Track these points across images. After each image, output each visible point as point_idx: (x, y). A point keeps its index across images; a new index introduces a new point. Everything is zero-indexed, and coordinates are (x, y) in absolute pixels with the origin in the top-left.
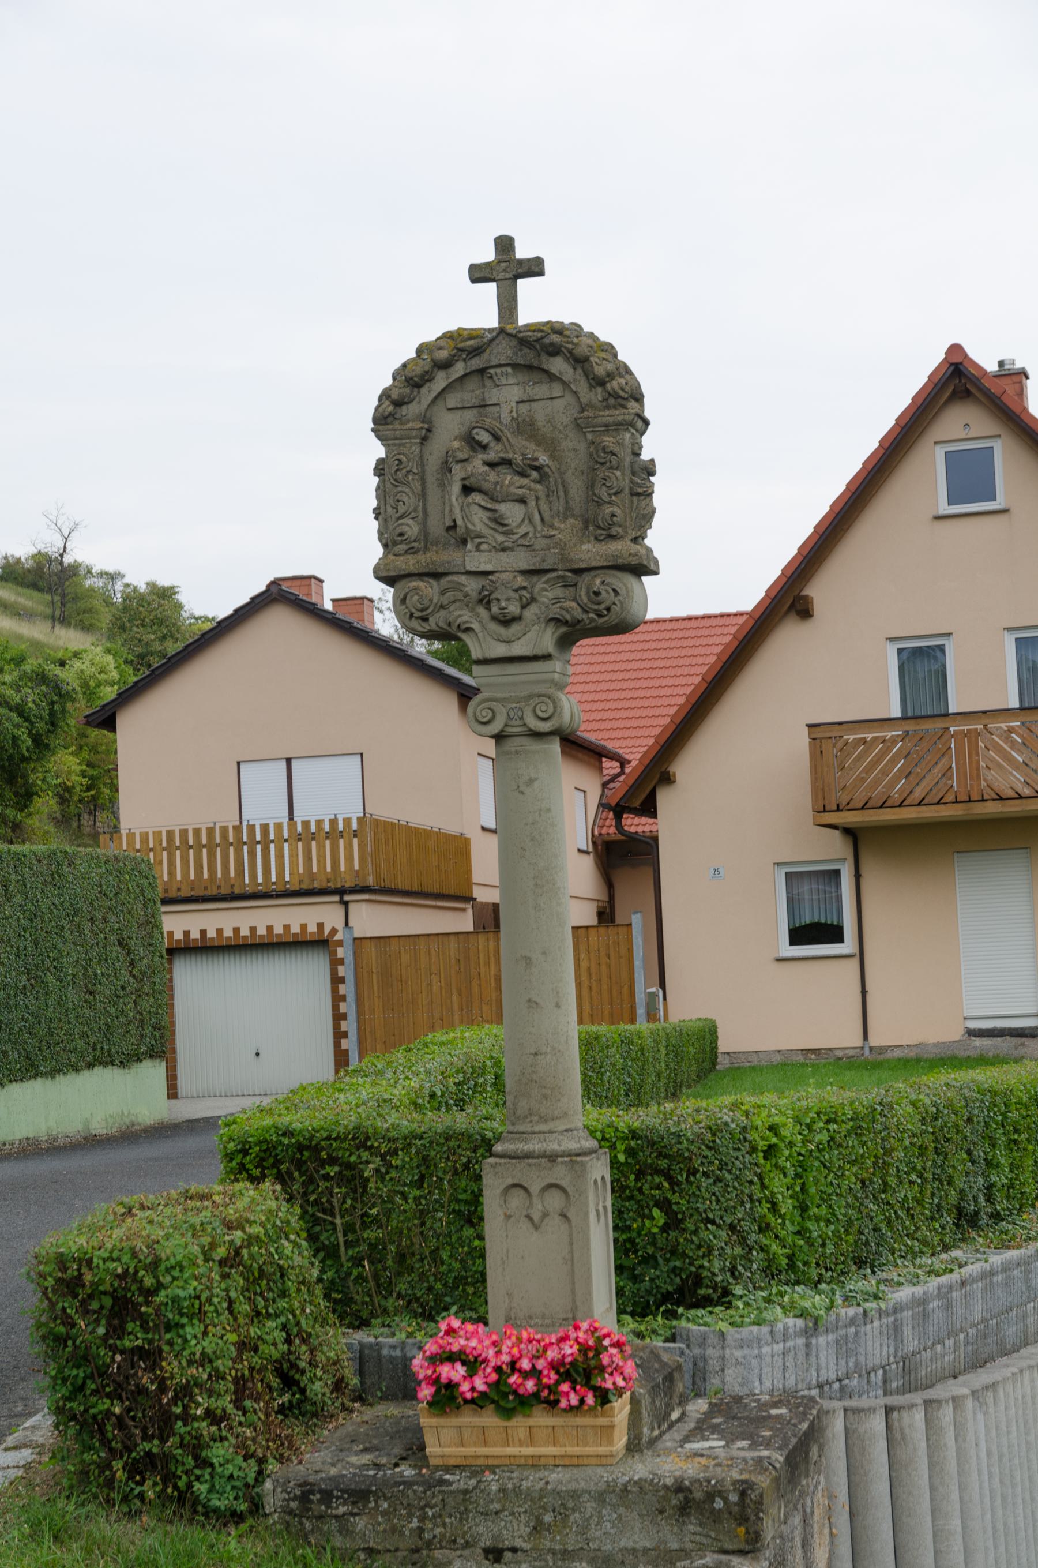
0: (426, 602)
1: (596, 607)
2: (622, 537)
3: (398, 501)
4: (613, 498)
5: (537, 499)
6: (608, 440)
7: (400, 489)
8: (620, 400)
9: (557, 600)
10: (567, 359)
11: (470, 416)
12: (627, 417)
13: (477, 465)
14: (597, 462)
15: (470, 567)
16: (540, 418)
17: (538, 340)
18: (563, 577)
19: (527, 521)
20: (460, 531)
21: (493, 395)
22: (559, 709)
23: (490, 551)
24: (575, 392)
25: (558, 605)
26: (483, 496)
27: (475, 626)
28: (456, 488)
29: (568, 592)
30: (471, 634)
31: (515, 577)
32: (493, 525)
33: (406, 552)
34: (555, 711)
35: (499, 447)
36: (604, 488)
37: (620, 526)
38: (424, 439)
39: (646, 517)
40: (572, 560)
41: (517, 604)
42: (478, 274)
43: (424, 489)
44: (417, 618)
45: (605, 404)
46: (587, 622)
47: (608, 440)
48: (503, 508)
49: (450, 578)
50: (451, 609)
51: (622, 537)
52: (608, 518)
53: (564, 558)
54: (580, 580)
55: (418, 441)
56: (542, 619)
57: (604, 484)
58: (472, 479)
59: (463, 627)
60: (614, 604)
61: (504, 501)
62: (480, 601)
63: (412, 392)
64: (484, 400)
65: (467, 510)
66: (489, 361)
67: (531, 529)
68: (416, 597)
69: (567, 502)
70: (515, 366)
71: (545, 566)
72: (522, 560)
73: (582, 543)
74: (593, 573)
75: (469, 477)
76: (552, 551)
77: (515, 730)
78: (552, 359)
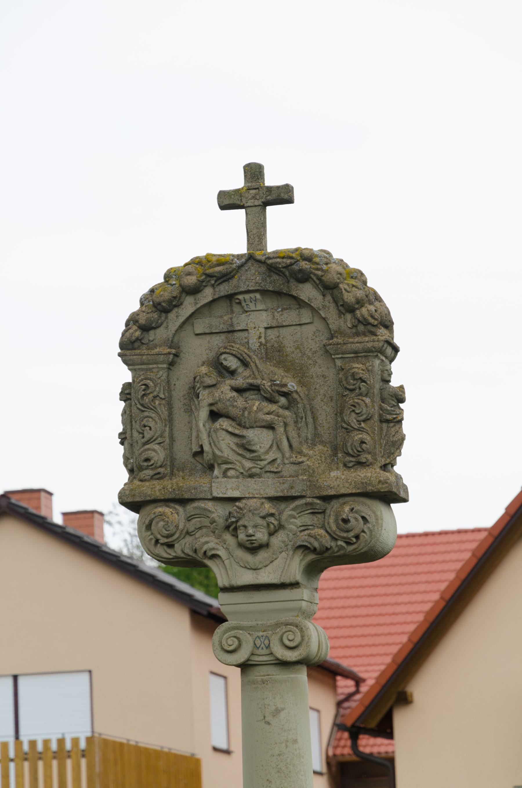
0: (172, 528)
1: (345, 535)
2: (371, 464)
3: (145, 426)
4: (363, 425)
5: (286, 425)
6: (357, 367)
7: (146, 414)
8: (369, 327)
9: (305, 527)
10: (316, 286)
11: (218, 341)
12: (376, 344)
13: (225, 391)
14: (346, 389)
16: (289, 346)
17: (287, 267)
18: (311, 504)
19: (275, 448)
20: (207, 457)
21: (242, 321)
22: (306, 638)
23: (237, 477)
24: (324, 319)
25: (306, 532)
26: (231, 422)
27: (222, 553)
28: (203, 414)
29: (317, 519)
30: (218, 561)
31: (263, 503)
33: (152, 478)
34: (302, 640)
35: (247, 373)
36: (353, 414)
37: (369, 453)
38: (172, 364)
40: (320, 487)
41: (265, 531)
42: (228, 201)
44: (162, 544)
45: (354, 330)
46: (336, 549)
47: (357, 367)
48: (251, 434)
49: (196, 504)
50: (197, 535)
51: (371, 464)
52: (357, 444)
55: (165, 366)
56: (289, 547)
57: (353, 411)
59: (210, 553)
60: (363, 531)
62: (227, 528)
63: (160, 317)
64: (232, 325)
67: (279, 455)
68: (162, 523)
69: (316, 428)
70: (264, 292)
71: (294, 493)
72: (270, 487)
74: (341, 500)
75: (216, 403)
76: (300, 477)
78: (301, 285)
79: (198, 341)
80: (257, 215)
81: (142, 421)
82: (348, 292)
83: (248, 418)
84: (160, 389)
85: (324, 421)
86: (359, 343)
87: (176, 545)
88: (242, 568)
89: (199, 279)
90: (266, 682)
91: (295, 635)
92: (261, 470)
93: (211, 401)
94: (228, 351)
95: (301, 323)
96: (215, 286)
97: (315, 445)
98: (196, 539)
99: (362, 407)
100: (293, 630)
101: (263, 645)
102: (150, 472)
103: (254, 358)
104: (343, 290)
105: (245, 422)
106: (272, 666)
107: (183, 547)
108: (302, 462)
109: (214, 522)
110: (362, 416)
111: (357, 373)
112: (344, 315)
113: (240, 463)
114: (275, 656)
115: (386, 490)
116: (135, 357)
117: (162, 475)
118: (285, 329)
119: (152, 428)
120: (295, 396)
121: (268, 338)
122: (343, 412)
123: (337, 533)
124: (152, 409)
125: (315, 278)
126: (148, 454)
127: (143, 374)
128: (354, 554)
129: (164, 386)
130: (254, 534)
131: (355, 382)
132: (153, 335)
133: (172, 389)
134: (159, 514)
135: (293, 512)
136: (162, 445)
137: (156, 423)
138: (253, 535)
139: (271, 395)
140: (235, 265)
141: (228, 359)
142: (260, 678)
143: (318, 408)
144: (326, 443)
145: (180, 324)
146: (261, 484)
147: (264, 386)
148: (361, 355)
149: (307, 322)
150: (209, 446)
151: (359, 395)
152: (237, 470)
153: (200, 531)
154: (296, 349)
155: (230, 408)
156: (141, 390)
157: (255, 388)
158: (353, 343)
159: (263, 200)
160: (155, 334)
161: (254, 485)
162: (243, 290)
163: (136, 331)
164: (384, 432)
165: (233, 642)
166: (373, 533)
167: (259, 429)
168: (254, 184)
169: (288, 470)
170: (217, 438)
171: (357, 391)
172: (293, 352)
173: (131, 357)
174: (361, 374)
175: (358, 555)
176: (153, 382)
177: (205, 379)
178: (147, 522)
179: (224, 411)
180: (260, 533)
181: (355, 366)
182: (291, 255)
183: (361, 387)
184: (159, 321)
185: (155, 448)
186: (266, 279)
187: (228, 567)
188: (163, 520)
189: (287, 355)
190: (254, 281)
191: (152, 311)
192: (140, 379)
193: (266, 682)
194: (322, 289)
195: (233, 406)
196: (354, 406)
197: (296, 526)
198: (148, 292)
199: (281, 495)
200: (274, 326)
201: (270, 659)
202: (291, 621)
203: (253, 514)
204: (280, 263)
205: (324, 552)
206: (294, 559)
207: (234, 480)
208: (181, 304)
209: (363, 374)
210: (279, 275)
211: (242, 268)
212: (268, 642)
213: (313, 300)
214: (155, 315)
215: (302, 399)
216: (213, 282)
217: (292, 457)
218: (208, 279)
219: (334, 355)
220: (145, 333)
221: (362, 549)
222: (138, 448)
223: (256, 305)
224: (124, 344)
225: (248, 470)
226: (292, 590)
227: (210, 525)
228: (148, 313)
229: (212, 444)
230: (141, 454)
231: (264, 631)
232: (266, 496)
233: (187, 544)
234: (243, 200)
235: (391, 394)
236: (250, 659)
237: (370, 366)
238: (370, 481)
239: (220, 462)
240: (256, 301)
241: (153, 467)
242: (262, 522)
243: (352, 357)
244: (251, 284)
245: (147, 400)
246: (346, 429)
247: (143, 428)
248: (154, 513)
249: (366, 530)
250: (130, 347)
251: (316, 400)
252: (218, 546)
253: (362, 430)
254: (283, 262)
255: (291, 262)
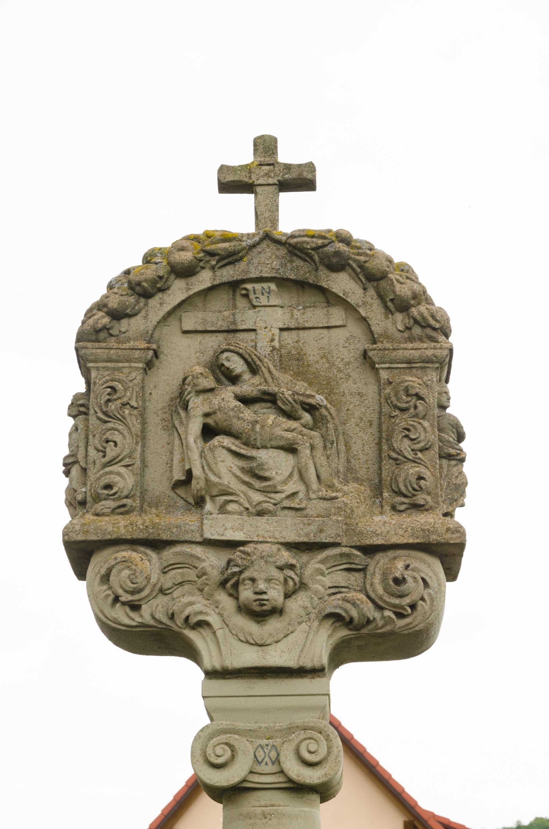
0: (141, 580)
1: (397, 601)
2: (431, 508)
3: (107, 441)
4: (420, 455)
5: (312, 447)
6: (412, 380)
7: (110, 425)
8: (428, 331)
9: (336, 589)
10: (355, 276)
11: (213, 342)
12: (438, 352)
13: (227, 396)
14: (396, 407)
15: (212, 532)
16: (312, 352)
17: (315, 249)
18: (348, 555)
19: (296, 476)
20: (197, 485)
21: (247, 318)
23: (240, 514)
24: (364, 319)
25: (338, 596)
26: (233, 440)
27: (213, 619)
28: (195, 427)
29: (355, 578)
30: (206, 632)
31: (279, 550)
32: (247, 478)
33: (113, 511)
34: (329, 753)
35: (257, 380)
36: (407, 442)
37: (429, 494)
38: (149, 365)
39: (456, 492)
40: (362, 533)
41: (281, 588)
43: (143, 431)
44: (124, 603)
45: (406, 335)
46: (380, 623)
47: (412, 380)
48: (263, 455)
49: (178, 548)
50: (175, 594)
51: (431, 508)
52: (414, 480)
53: (350, 530)
54: (372, 563)
55: (141, 365)
56: (313, 616)
57: (406, 436)
58: (219, 415)
59: (194, 620)
60: (422, 599)
61: (265, 447)
62: (223, 584)
63: (138, 302)
64: (234, 322)
65: (209, 455)
66: (248, 272)
67: (301, 488)
68: (126, 572)
69: (348, 461)
70: (282, 282)
71: (324, 538)
72: (291, 529)
73: (372, 514)
74: (391, 554)
75: (215, 413)
76: (334, 518)
77: (263, 779)
78: (334, 275)
79: (186, 341)
80: (271, 196)
81: (104, 434)
82: (401, 283)
83: (260, 434)
84: (132, 394)
85: (360, 452)
86: (411, 350)
87: (144, 607)
88: (241, 643)
89: (197, 256)
90: (269, 817)
91: (318, 745)
92: (275, 507)
93: (207, 409)
94: (232, 348)
95: (329, 325)
96: (216, 269)
97: (348, 482)
98: (173, 599)
99: (419, 431)
100: (315, 737)
101: (267, 759)
102: (112, 504)
103: (267, 363)
104: (395, 281)
105: (255, 439)
106: (281, 791)
107: (154, 609)
108: (336, 498)
109: (205, 574)
110: (418, 443)
111: (412, 387)
112: (392, 315)
113: (245, 494)
114: (286, 775)
115: (457, 541)
116: (99, 351)
117: (129, 507)
118: (307, 332)
119: (119, 443)
120: (324, 412)
121: (282, 343)
122: (392, 438)
123: (385, 598)
124: (119, 419)
125: (354, 265)
126: (110, 478)
127: (109, 375)
128: (406, 632)
129: (137, 392)
130: (265, 591)
131: (409, 399)
132: (127, 326)
133: (147, 399)
134: (123, 559)
135: (322, 566)
136: (130, 468)
137: (124, 437)
138: (265, 593)
139: (293, 407)
140: (245, 243)
141: (232, 359)
142: (259, 810)
143: (352, 435)
144: (362, 480)
145: (164, 313)
146: (276, 524)
147: (283, 394)
148: (416, 365)
149: (338, 324)
150: (201, 469)
151: (414, 416)
152: (240, 504)
153: (180, 588)
154: (321, 358)
155: (235, 420)
156: (106, 393)
157: (269, 399)
158: (406, 349)
159: (279, 178)
160: (129, 325)
161: (266, 525)
162: (254, 276)
163: (103, 317)
164: (445, 470)
165: (224, 751)
166: (435, 602)
167: (275, 450)
168: (267, 159)
169: (315, 507)
170: (215, 458)
171: (412, 410)
172: (317, 362)
173: (94, 351)
174: (417, 389)
175: (414, 632)
176: (123, 386)
177: (200, 380)
178: (103, 571)
179: (225, 424)
180: (275, 591)
181: (408, 379)
182: (323, 234)
183: (418, 405)
184: (137, 308)
185: (121, 471)
186: (286, 265)
187: (221, 640)
188: (129, 567)
189: (308, 366)
190: (269, 265)
191: (127, 294)
192: (104, 380)
193: (269, 817)
194: (363, 280)
195: (239, 418)
196: (408, 430)
197: (323, 586)
198: (122, 273)
199: (306, 540)
200: (293, 327)
201: (273, 781)
202: (312, 724)
203: (266, 562)
204: (308, 243)
205: (363, 626)
206: (319, 633)
207: (236, 517)
208: (168, 288)
209: (419, 388)
210: (304, 260)
211: (253, 250)
212: (276, 755)
213: (350, 295)
214: (132, 300)
215: (333, 418)
216: (214, 263)
217: (322, 491)
218: (208, 258)
219: (378, 364)
220: (114, 322)
221: (417, 625)
222: (95, 471)
223: (268, 299)
224: (85, 334)
225: (256, 505)
226: (312, 680)
227: (196, 579)
228: (122, 295)
229: (206, 468)
230: (99, 479)
231: (269, 739)
232: (282, 540)
233: (160, 607)
234: (252, 177)
235: (452, 423)
236: (248, 779)
237: (429, 380)
238: (433, 527)
239: (215, 493)
240: (269, 293)
241: (116, 496)
242: (279, 575)
243: (404, 368)
244: (266, 269)
245: (113, 407)
246: (396, 460)
247: (105, 445)
248: (115, 558)
249: (426, 597)
250: (93, 338)
251: (348, 425)
252: (205, 609)
253: (419, 461)
254: (313, 242)
255: (323, 243)
